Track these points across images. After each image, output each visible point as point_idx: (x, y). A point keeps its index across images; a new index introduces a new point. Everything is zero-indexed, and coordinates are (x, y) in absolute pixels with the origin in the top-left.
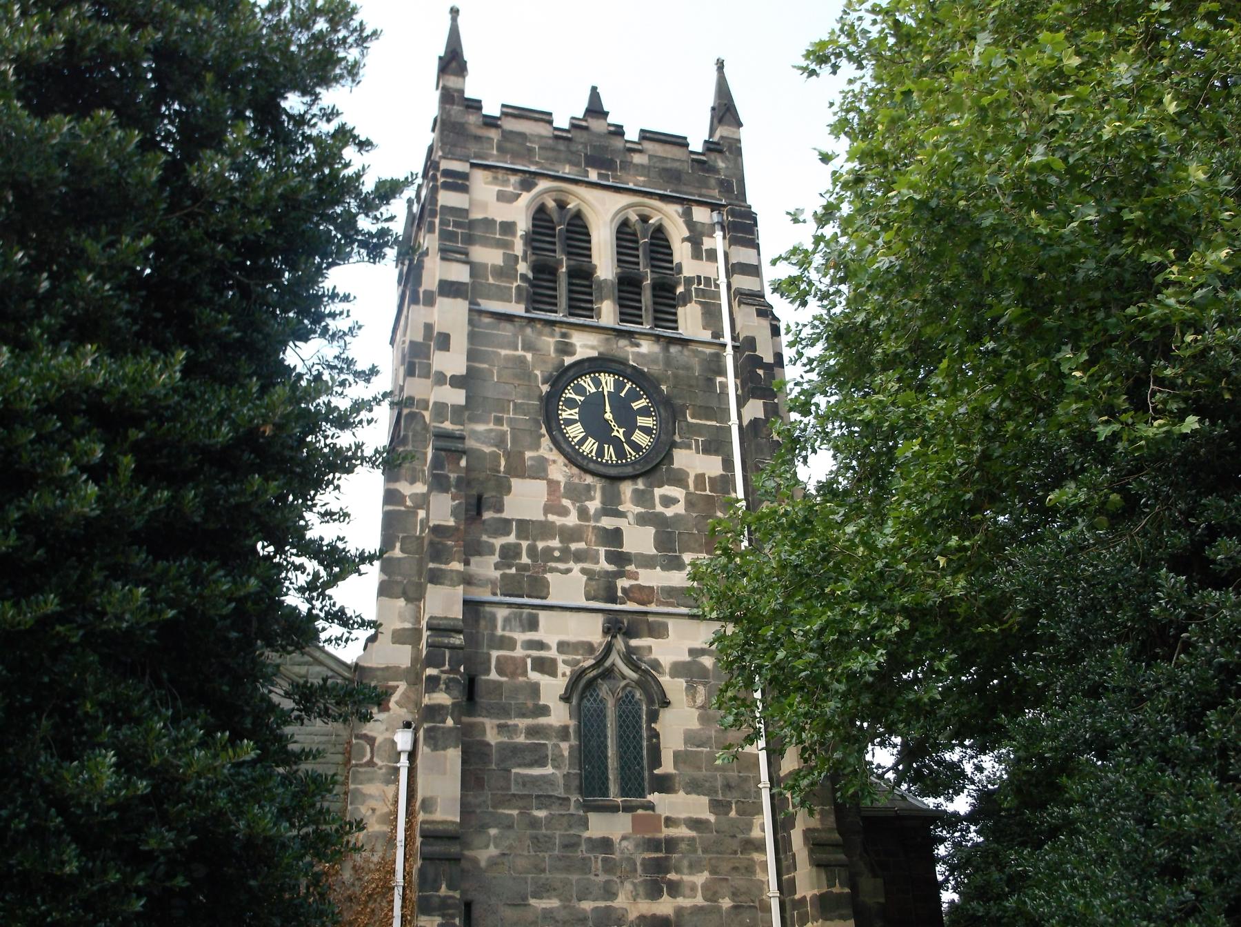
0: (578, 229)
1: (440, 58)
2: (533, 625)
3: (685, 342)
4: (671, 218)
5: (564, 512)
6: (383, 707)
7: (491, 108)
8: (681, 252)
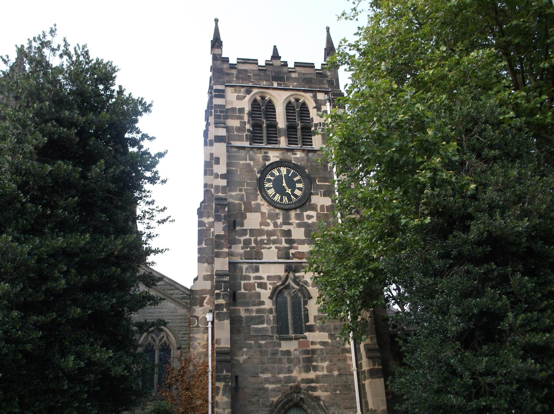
0: (270, 106)
3: (315, 151)
4: (308, 99)
6: (201, 305)
7: (233, 61)
8: (313, 113)
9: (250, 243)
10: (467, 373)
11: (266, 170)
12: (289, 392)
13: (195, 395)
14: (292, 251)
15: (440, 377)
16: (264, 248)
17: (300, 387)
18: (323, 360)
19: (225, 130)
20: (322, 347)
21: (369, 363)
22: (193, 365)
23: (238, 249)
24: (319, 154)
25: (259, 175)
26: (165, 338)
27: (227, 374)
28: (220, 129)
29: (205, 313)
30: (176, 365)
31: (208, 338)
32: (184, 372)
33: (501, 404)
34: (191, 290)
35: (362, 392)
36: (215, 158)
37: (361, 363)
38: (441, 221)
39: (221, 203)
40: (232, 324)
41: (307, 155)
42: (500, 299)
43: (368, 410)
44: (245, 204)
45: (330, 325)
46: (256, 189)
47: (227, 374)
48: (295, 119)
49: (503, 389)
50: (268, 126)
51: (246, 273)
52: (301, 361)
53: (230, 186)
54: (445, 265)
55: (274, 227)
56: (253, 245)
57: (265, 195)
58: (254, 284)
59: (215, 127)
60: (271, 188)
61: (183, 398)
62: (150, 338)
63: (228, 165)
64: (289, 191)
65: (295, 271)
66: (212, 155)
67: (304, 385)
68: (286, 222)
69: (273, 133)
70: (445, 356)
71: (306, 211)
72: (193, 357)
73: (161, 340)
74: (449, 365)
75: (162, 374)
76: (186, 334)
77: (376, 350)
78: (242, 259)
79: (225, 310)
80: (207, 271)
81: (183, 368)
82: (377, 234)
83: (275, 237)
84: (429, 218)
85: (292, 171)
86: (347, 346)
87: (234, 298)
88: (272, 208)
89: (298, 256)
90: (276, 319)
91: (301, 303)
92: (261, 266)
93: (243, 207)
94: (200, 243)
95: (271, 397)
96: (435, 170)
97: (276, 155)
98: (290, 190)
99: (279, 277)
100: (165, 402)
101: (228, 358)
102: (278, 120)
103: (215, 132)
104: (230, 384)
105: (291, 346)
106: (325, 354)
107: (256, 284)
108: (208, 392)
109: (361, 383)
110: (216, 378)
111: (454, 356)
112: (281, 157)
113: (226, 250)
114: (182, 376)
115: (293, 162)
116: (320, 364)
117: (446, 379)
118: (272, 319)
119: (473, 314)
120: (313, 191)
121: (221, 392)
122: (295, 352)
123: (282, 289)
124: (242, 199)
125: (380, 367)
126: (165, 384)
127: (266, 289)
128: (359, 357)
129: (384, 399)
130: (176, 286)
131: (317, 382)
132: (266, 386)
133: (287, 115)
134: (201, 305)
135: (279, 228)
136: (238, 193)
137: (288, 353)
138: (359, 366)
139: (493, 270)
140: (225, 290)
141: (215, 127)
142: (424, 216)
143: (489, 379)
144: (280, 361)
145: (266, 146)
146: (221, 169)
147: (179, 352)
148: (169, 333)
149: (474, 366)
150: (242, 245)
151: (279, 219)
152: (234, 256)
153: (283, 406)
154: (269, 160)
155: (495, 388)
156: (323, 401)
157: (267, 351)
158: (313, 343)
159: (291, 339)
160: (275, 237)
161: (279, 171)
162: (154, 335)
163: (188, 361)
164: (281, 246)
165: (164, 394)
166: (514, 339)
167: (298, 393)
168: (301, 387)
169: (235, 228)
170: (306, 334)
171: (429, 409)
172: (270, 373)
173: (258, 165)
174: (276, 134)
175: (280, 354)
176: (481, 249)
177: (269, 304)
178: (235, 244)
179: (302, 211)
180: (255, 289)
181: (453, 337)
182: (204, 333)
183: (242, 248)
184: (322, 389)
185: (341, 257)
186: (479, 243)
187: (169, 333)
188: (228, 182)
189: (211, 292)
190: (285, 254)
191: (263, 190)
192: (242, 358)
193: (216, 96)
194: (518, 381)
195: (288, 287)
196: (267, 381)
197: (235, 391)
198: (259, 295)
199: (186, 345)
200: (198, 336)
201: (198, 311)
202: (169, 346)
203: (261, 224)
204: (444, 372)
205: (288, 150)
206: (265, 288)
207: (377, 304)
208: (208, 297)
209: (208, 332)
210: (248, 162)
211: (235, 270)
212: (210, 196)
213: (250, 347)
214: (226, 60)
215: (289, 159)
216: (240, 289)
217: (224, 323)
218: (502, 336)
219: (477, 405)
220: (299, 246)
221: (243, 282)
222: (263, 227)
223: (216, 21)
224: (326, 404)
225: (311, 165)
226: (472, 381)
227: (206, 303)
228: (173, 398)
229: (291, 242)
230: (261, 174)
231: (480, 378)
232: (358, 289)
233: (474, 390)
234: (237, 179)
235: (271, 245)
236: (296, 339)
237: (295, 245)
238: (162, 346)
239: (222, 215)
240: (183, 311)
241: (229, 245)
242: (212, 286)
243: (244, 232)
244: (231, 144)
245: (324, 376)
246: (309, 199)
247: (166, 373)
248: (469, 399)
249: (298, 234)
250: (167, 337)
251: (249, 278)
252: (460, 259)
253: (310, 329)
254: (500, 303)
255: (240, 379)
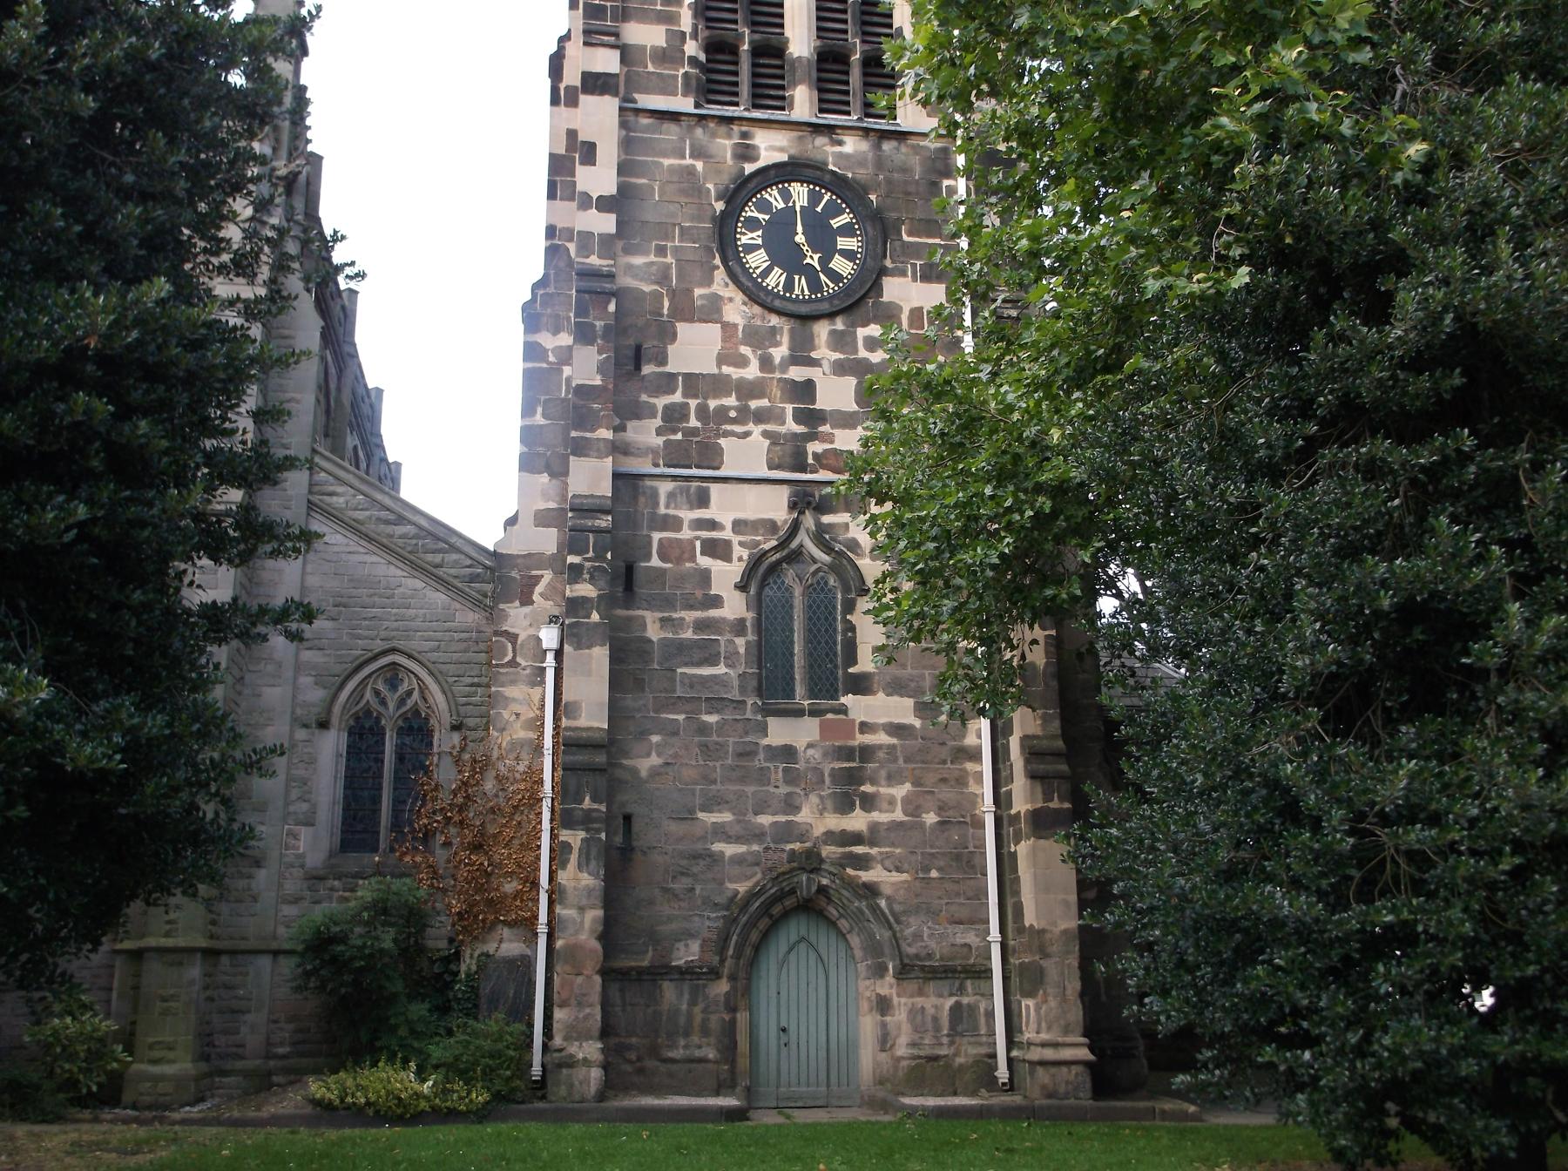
3: (902, 136)
6: (527, 600)
9: (686, 417)
10: (1338, 814)
11: (742, 190)
12: (786, 867)
13: (500, 865)
14: (814, 447)
15: (1241, 825)
16: (727, 434)
17: (819, 854)
18: (893, 779)
19: (616, 54)
20: (894, 741)
21: (1033, 793)
22: (497, 777)
23: (646, 433)
24: (913, 147)
25: (720, 206)
26: (416, 694)
27: (596, 806)
28: (601, 51)
29: (535, 624)
30: (446, 774)
31: (543, 699)
32: (467, 797)
33: (1450, 923)
34: (495, 555)
35: (1008, 877)
36: (584, 143)
37: (1009, 793)
38: (1288, 282)
39: (597, 288)
40: (614, 659)
41: (878, 147)
42: (1481, 559)
43: (1021, 930)
44: (673, 294)
45: (922, 677)
46: (709, 250)
47: (596, 806)
48: (845, 32)
49: (1462, 871)
50: (758, 51)
51: (667, 507)
52: (827, 780)
53: (627, 235)
54: (1290, 439)
55: (762, 369)
56: (694, 422)
57: (738, 270)
58: (691, 542)
59: (586, 44)
60: (757, 247)
61: (463, 873)
62: (368, 695)
63: (623, 169)
64: (813, 260)
65: (823, 507)
66: (572, 134)
67: (833, 848)
68: (802, 355)
70: (1263, 754)
71: (864, 325)
72: (495, 754)
73: (402, 702)
74: (1274, 785)
75: (405, 802)
76: (479, 685)
77: (1056, 754)
78: (656, 465)
79: (595, 617)
80: (547, 499)
81: (465, 784)
82: (1068, 365)
83: (764, 402)
84: (1244, 270)
85: (827, 197)
86: (971, 740)
87: (626, 581)
88: (757, 309)
89: (832, 462)
90: (755, 651)
91: (835, 607)
92: (715, 489)
93: (666, 304)
94: (528, 411)
95: (731, 881)
96: (1280, 96)
97: (778, 144)
98: (816, 257)
99: (772, 526)
100: (408, 880)
101: (600, 759)
102: (788, 32)
103: (581, 60)
104: (603, 836)
105: (799, 734)
106: (901, 761)
107: (698, 544)
108: (538, 858)
109: (1005, 851)
110: (564, 819)
111: (1296, 754)
112: (793, 152)
113: (605, 434)
114: (462, 809)
115: (831, 167)
116: (882, 790)
117: (1263, 831)
118: (742, 650)
119: (1378, 614)
120: (888, 263)
121: (574, 858)
122: (810, 752)
123: (779, 563)
124: (663, 277)
125: (1067, 805)
126: (413, 831)
127: (728, 559)
128: (1004, 774)
129: (1073, 898)
130: (453, 540)
131: (872, 844)
132: (717, 847)
133: (819, 19)
134: (527, 600)
135: (778, 375)
136: (652, 258)
137: (788, 752)
138: (1002, 800)
139: (1464, 458)
140: (599, 556)
141: (586, 44)
142: (1228, 264)
143: (1417, 835)
144: (763, 777)
145: (746, 114)
146: (599, 179)
147: (456, 738)
148: (429, 680)
149: (1366, 791)
150: (658, 422)
151: (778, 344)
152: (632, 454)
153: (766, 909)
154: (754, 159)
155: (1434, 866)
156: (888, 898)
157: (721, 746)
158: (865, 727)
159: (799, 713)
160: (764, 402)
161: (786, 196)
162: (381, 686)
163: (481, 765)
164: (782, 429)
165: (407, 859)
166: (1517, 701)
167: (811, 872)
168: (824, 854)
169: (638, 368)
170: (848, 700)
171: (1197, 930)
172: (730, 810)
173: (719, 172)
174: (782, 77)
175: (761, 756)
176: (1425, 381)
177: (734, 606)
178: (638, 417)
179: (854, 325)
180: (693, 558)
181: (1298, 690)
182: (533, 684)
183: (659, 432)
184: (887, 863)
185: (954, 447)
186: (1416, 363)
187: (429, 680)
188: (619, 224)
189: (556, 563)
190: (791, 455)
191: (730, 253)
192: (646, 764)
194: (1518, 846)
195: (796, 556)
196: (721, 832)
197: (619, 860)
198: (705, 576)
199: (474, 720)
200: (511, 691)
201: (517, 617)
202: (427, 719)
203: (722, 360)
204: (1255, 809)
205: (817, 129)
206: (727, 558)
207: (1055, 597)
208: (548, 576)
209: (543, 682)
210: (688, 161)
211: (635, 498)
212: (562, 264)
213: (672, 731)
215: (819, 157)
216: (648, 557)
217: (590, 656)
218: (1473, 693)
219: (1363, 923)
220: (836, 432)
221: (656, 536)
222: (726, 369)
224: (897, 908)
225: (889, 181)
226: (1351, 840)
227: (541, 595)
228: (435, 872)
229: (812, 418)
230: (727, 203)
231: (1383, 834)
232: (1011, 560)
233: (1356, 874)
234: (650, 216)
235: (751, 426)
236: (814, 713)
237: (826, 428)
238: (404, 717)
239: (599, 324)
240: (469, 617)
241: (617, 421)
242: (560, 546)
243: (667, 383)
244: (634, 101)
245: (896, 826)
246: (876, 288)
247: (416, 799)
248: (1336, 900)
249: (837, 393)
250: (422, 691)
251: (676, 524)
252: (1351, 419)
253: (860, 685)
254: (1478, 573)
255: (637, 826)
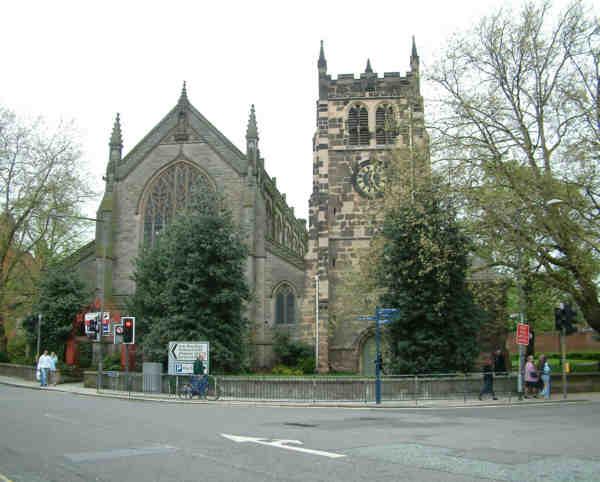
0: (365, 111)
1: (353, 75)
2: (350, 244)
5: (358, 211)
6: (311, 268)
7: (334, 77)
56: (348, 226)
66: (318, 158)
69: (366, 136)
146: (324, 170)
193: (322, 110)
200: (309, 289)
201: (310, 273)
214: (329, 77)
223: (322, 42)
